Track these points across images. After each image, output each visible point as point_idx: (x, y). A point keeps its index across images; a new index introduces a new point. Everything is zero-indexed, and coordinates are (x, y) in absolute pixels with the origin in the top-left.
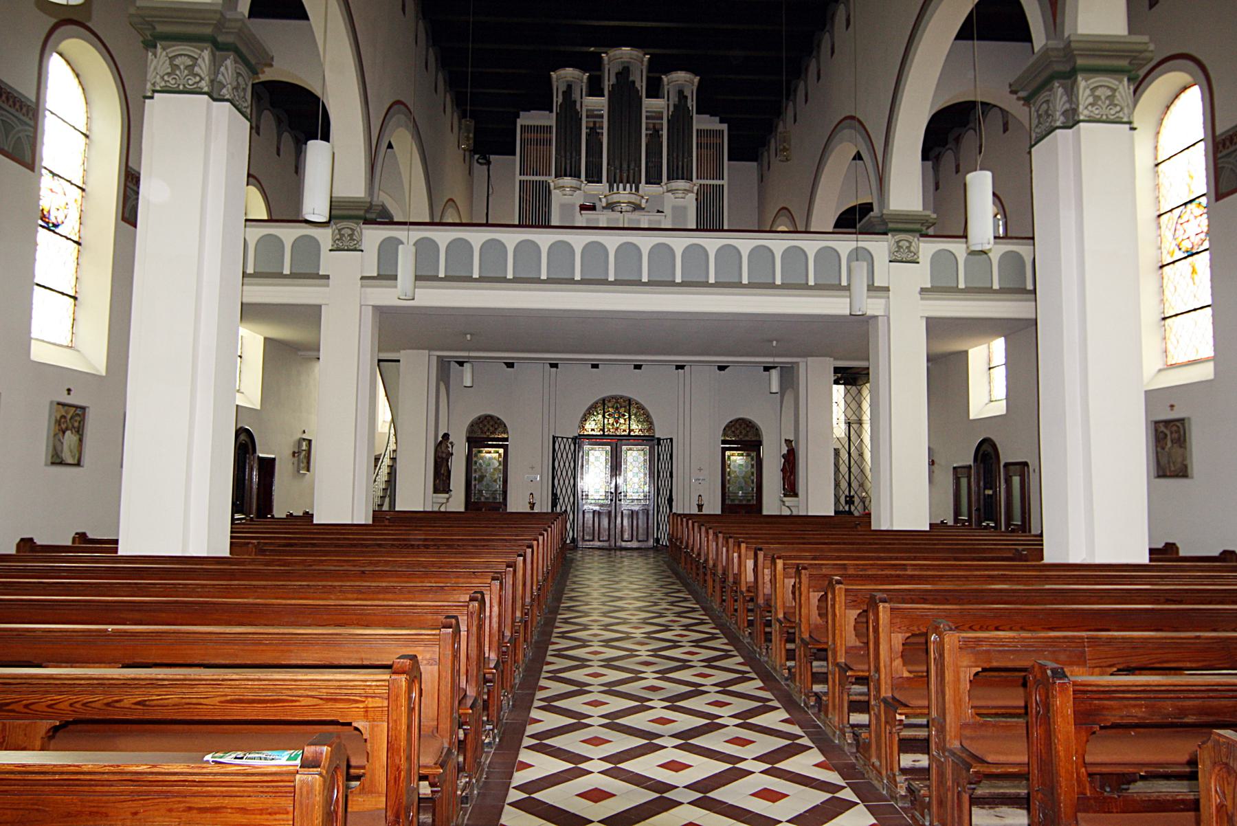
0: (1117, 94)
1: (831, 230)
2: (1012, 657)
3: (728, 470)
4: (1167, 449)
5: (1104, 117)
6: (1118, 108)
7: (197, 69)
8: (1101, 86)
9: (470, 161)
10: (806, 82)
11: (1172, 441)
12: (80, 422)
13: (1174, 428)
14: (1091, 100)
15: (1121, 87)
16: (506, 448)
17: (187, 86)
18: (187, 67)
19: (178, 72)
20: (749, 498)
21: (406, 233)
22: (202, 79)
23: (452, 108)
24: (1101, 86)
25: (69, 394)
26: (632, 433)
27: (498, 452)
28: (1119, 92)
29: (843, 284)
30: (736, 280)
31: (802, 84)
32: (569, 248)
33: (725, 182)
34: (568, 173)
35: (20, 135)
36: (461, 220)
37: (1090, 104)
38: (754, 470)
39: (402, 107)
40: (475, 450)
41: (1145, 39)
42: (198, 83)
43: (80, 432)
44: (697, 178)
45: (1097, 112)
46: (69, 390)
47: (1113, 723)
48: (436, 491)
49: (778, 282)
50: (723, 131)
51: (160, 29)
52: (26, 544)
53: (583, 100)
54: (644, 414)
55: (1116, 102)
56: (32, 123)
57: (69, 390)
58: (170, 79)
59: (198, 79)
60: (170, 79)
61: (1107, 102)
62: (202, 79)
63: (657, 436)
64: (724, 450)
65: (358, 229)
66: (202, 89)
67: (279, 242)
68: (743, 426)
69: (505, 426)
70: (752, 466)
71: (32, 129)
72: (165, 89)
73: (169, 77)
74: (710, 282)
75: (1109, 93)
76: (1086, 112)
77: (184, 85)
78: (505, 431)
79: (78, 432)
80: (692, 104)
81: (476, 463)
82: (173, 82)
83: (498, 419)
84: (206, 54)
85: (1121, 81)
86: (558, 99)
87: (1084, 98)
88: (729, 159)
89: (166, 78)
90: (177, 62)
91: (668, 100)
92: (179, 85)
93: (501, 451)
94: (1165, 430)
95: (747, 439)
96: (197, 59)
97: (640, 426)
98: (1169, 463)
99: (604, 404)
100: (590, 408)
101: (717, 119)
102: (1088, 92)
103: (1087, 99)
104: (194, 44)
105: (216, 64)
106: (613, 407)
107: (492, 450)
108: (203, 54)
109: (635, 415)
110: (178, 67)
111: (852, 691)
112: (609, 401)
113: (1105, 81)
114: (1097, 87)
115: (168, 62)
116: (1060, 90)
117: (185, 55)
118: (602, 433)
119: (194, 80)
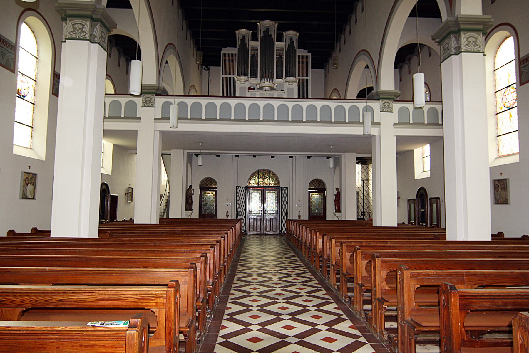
0: (478, 40)
1: (355, 98)
2: (433, 281)
3: (311, 201)
4: (499, 192)
5: (472, 50)
6: (478, 46)
7: (84, 30)
8: (471, 37)
9: (201, 69)
10: (345, 35)
11: (501, 188)
12: (34, 180)
13: (502, 183)
14: (466, 43)
15: (479, 37)
16: (216, 191)
17: (80, 37)
18: (80, 29)
19: (76, 31)
20: (321, 213)
21: (174, 99)
22: (86, 34)
23: (193, 46)
24: (471, 37)
25: (29, 168)
26: (270, 185)
27: (213, 193)
28: (479, 39)
29: (360, 121)
30: (315, 120)
31: (343, 36)
32: (243, 106)
33: (310, 78)
34: (243, 74)
35: (9, 58)
36: (197, 94)
37: (466, 45)
38: (323, 201)
39: (172, 46)
40: (203, 192)
41: (490, 16)
42: (85, 35)
43: (34, 185)
44: (298, 76)
45: (469, 48)
46: (29, 167)
47: (476, 309)
48: (186, 210)
49: (333, 120)
50: (309, 56)
51: (68, 12)
52: (11, 233)
53: (249, 43)
54: (275, 177)
55: (477, 44)
56: (14, 53)
57: (29, 167)
58: (73, 34)
59: (85, 34)
60: (73, 34)
61: (474, 44)
62: (86, 34)
63: (281, 186)
64: (310, 192)
65: (153, 98)
66: (86, 38)
67: (119, 104)
68: (318, 182)
69: (216, 182)
70: (322, 199)
71: (13, 55)
72: (70, 38)
73: (72, 33)
74: (304, 120)
75: (474, 40)
76: (464, 48)
77: (79, 36)
78: (216, 184)
79: (33, 185)
80: (296, 44)
81: (203, 198)
82: (74, 35)
83: (213, 179)
84: (88, 23)
85: (479, 35)
86: (238, 42)
87: (464, 42)
88: (312, 68)
89: (71, 33)
90: (76, 26)
91: (286, 43)
92: (77, 36)
93: (214, 193)
94: (498, 184)
95: (319, 187)
96: (84, 25)
97: (274, 182)
98: (500, 198)
99: (258, 173)
100: (252, 174)
101: (307, 51)
102: (465, 39)
103: (465, 42)
104: (83, 19)
105: (92, 27)
106: (262, 174)
107: (211, 192)
108: (87, 23)
109: (272, 177)
110: (76, 29)
111: (364, 295)
112: (261, 172)
113: (473, 35)
114: (469, 37)
115: (72, 26)
116: (453, 39)
117: (79, 24)
118: (257, 185)
119: (83, 34)
